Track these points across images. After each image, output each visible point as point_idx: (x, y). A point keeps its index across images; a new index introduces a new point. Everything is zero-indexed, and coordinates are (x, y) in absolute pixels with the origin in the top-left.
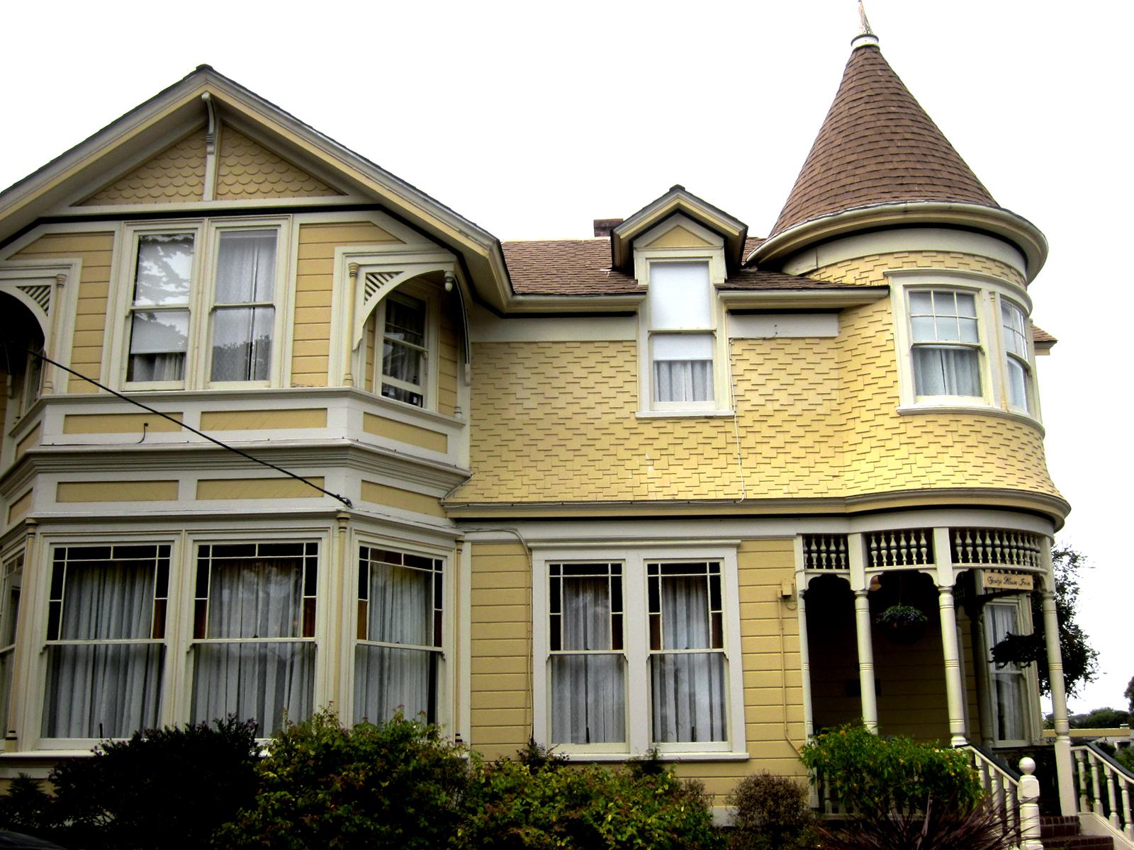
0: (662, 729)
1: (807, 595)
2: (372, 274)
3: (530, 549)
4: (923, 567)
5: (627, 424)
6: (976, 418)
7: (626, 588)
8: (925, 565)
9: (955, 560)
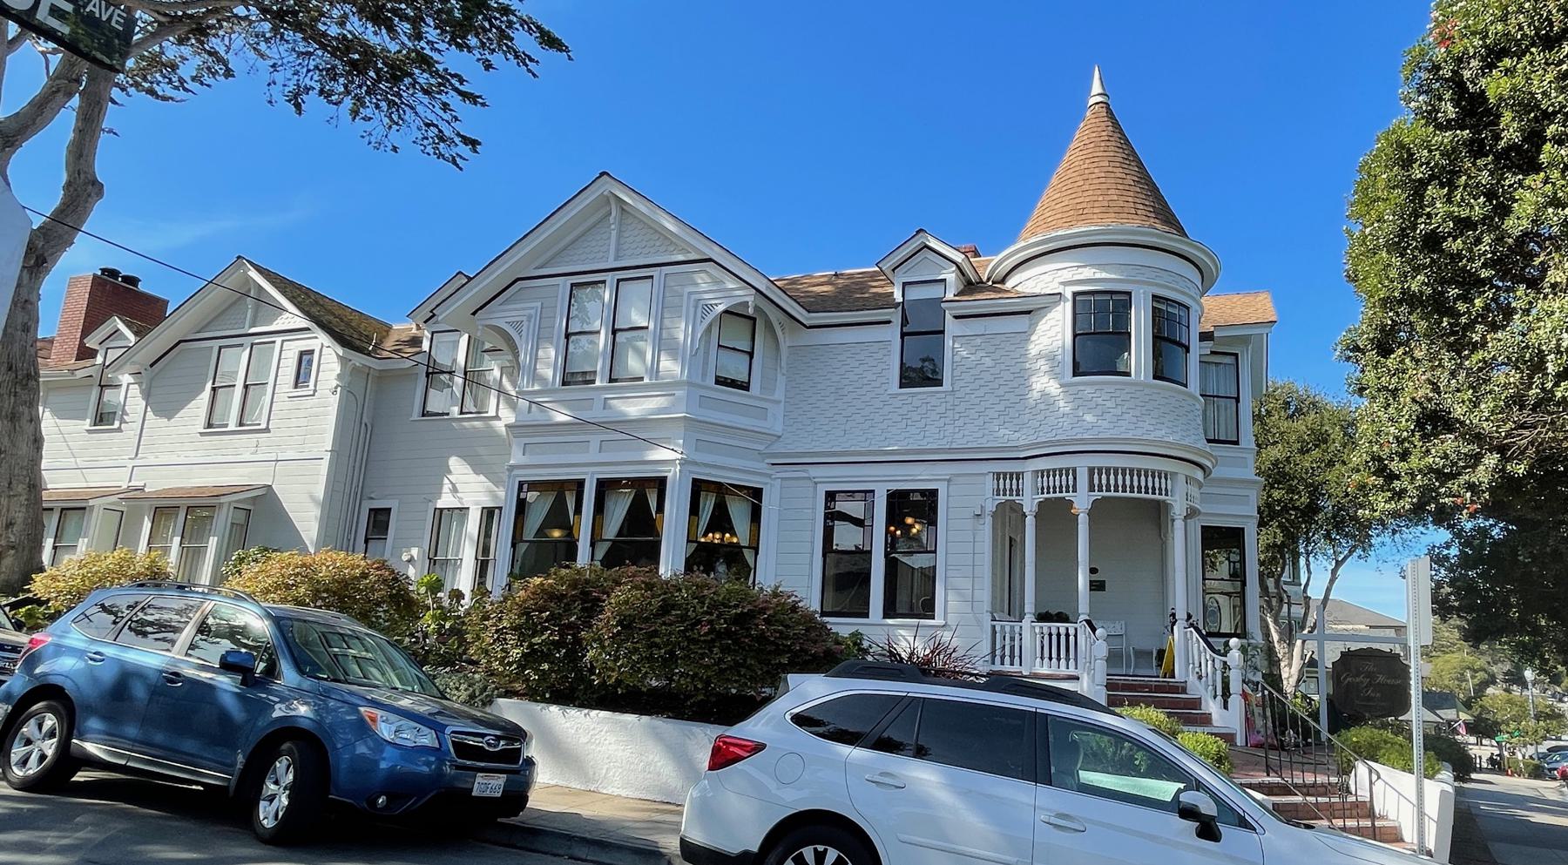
0: (486, 532)
1: (994, 515)
2: (706, 305)
3: (816, 483)
4: (1068, 496)
5: (882, 398)
6: (1097, 387)
7: (686, 505)
8: (1071, 494)
9: (1092, 489)
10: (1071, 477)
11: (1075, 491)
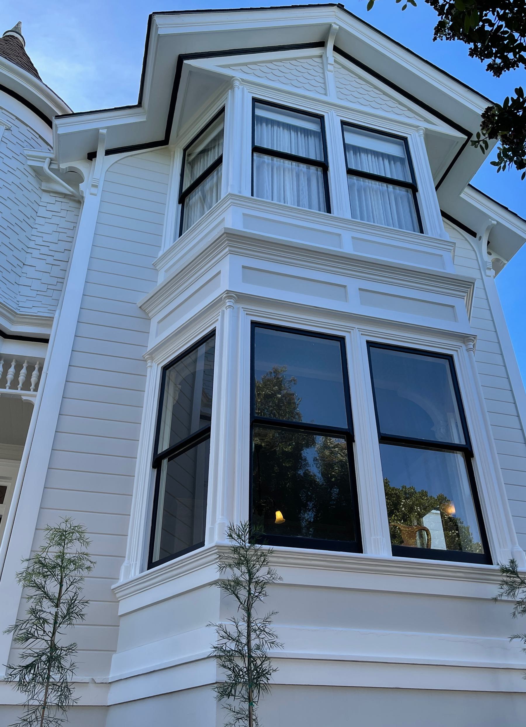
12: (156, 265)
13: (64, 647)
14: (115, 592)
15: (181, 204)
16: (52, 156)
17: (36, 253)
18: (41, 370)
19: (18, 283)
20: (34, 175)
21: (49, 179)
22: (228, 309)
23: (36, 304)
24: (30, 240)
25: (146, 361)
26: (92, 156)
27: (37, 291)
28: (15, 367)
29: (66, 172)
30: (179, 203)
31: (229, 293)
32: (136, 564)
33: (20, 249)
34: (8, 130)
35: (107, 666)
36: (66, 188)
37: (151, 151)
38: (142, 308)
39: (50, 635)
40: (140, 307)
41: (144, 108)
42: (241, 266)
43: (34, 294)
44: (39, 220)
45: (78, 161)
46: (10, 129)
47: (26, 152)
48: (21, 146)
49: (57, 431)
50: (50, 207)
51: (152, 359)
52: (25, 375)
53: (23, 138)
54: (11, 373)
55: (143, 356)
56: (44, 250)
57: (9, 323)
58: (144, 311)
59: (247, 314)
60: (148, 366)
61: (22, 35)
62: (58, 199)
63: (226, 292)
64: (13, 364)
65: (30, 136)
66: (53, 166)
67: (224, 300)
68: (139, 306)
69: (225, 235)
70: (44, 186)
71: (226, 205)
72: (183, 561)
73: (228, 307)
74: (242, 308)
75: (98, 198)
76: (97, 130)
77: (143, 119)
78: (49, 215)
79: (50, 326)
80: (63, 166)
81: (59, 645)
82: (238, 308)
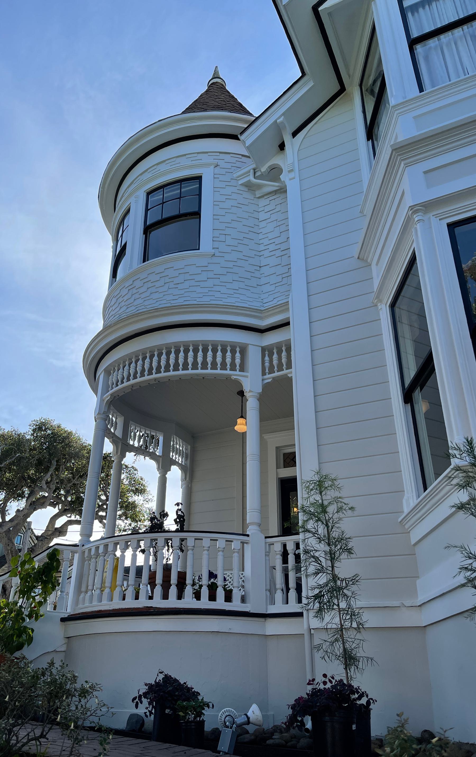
10: (238, 355)
11: (242, 369)
12: (362, 211)
13: (347, 578)
14: (403, 524)
15: (371, 140)
16: (254, 166)
17: (266, 253)
18: (289, 350)
19: (259, 285)
20: (246, 189)
21: (259, 187)
22: (418, 224)
23: (276, 296)
24: (259, 244)
25: (376, 305)
26: (282, 147)
27: (275, 284)
28: (277, 353)
29: (268, 173)
30: (368, 140)
31: (413, 208)
32: (413, 496)
33: (254, 256)
34: (216, 166)
35: (414, 593)
36: (272, 186)
37: (333, 107)
38: (360, 258)
39: (330, 569)
40: (358, 258)
41: (308, 74)
42: (423, 173)
43: (273, 288)
44: (262, 225)
45: (273, 158)
46: (218, 165)
47: (235, 175)
48: (230, 172)
49: (315, 395)
50: (267, 209)
51: (381, 301)
52: (286, 357)
53: (229, 166)
54: (284, 357)
55: (372, 302)
56: (272, 247)
57: (260, 320)
58: (363, 259)
59: (440, 220)
60: (379, 309)
61: (221, 77)
62: (271, 198)
63: (410, 209)
64: (275, 351)
65: (234, 160)
66: (258, 174)
67: (411, 217)
68: (357, 258)
69: (394, 152)
70: (258, 194)
71: (394, 121)
72: (438, 487)
73: (417, 223)
74: (433, 216)
75: (297, 179)
76: (276, 121)
77: (311, 84)
78: (267, 215)
79: (288, 309)
80: (264, 169)
81: (341, 576)
82: (429, 218)
